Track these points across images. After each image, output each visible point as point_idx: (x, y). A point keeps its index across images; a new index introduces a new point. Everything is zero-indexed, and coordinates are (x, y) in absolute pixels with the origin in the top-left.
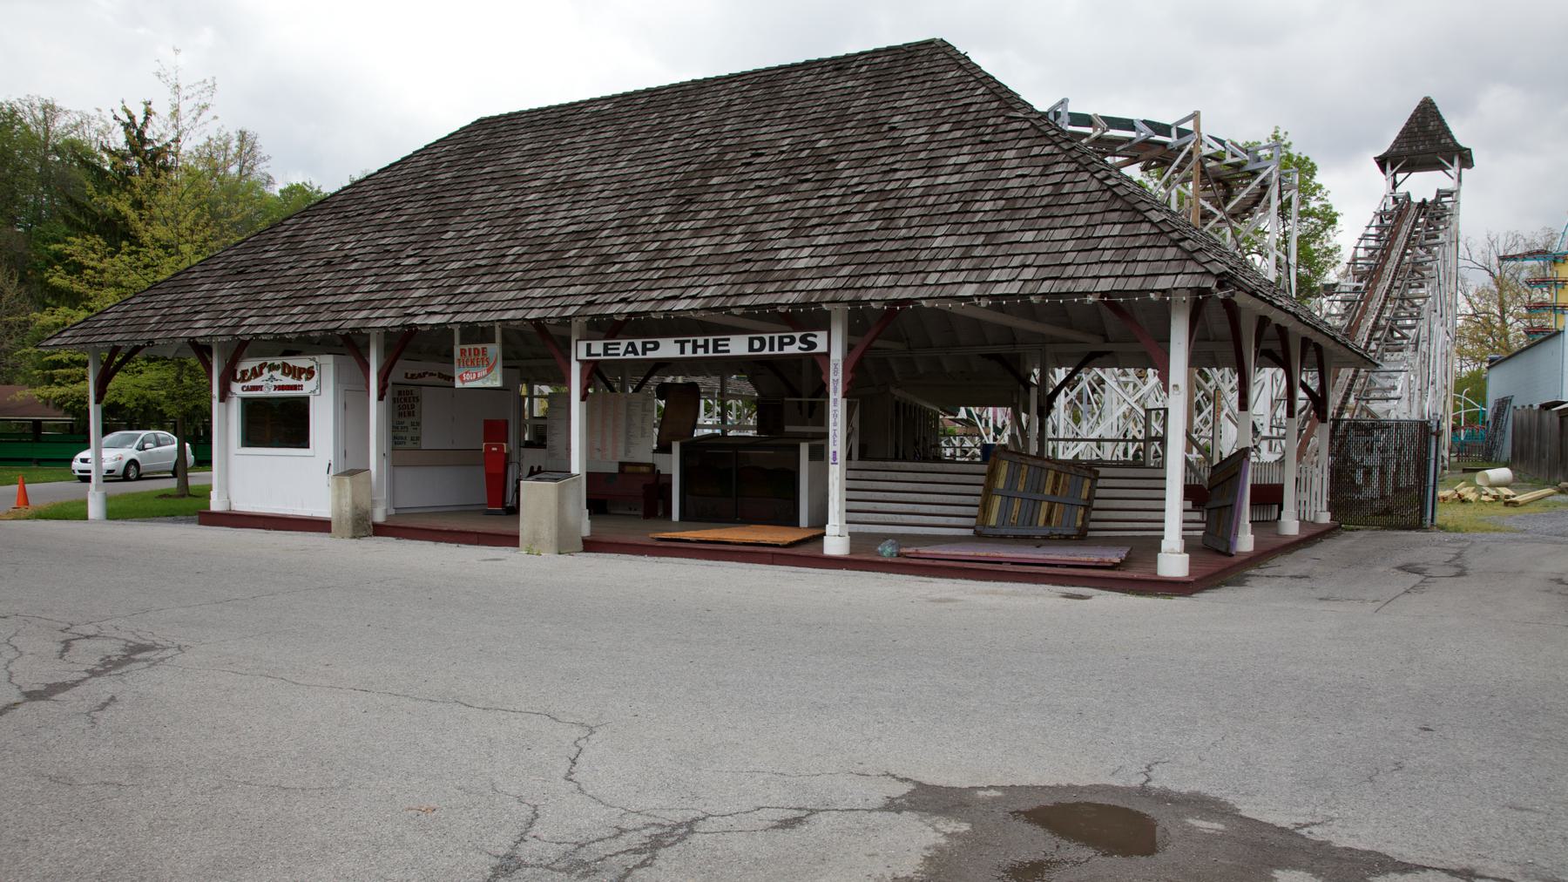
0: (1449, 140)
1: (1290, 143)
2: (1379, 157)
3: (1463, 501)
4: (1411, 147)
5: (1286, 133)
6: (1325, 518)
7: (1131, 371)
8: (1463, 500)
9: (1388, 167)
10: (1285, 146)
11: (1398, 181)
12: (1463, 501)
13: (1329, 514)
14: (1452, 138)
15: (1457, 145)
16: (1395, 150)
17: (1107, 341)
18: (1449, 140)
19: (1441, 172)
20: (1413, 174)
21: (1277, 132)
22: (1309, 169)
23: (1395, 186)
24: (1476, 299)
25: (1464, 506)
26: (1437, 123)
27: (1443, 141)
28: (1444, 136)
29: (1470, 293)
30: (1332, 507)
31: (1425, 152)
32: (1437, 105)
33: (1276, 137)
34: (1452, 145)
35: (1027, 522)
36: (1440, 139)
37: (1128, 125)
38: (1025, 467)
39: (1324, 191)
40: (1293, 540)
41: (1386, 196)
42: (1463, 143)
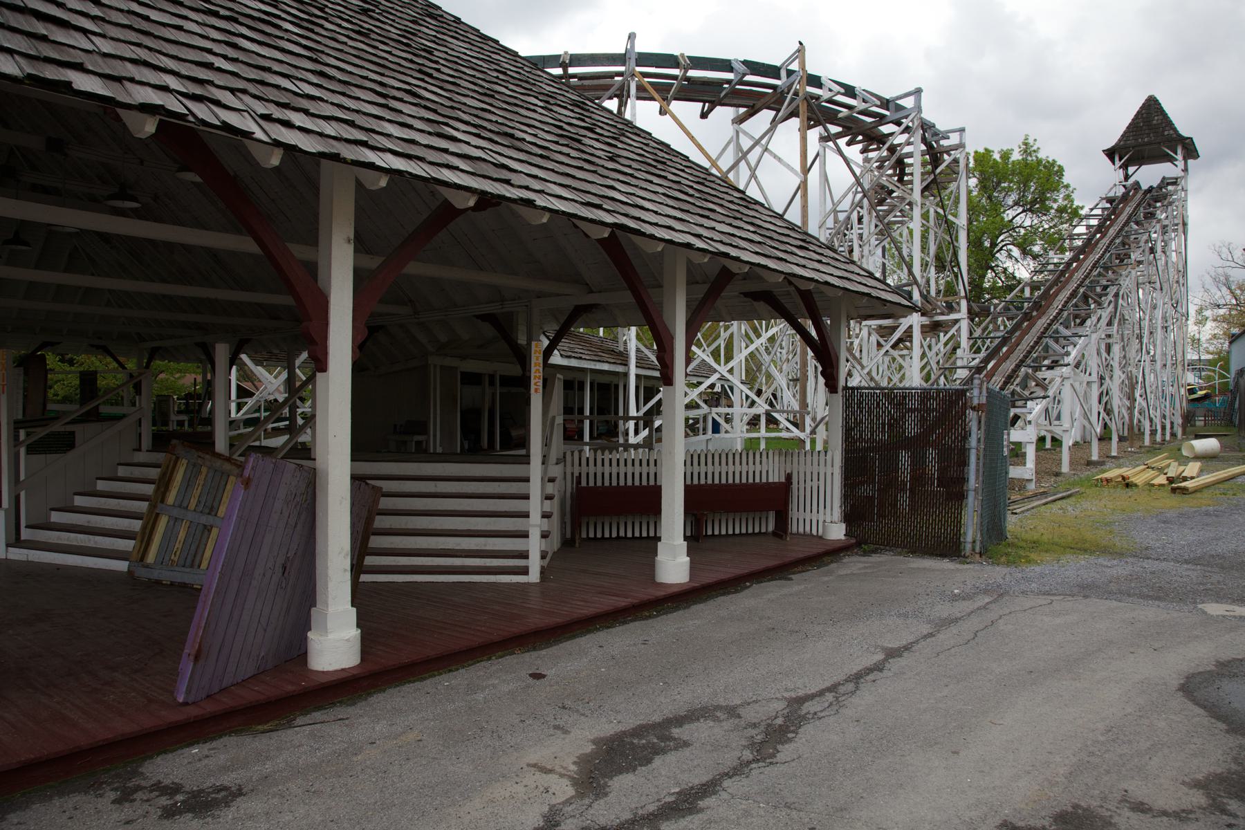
0: (1171, 132)
1: (1038, 148)
2: (1108, 150)
3: (1127, 485)
4: (1136, 140)
5: (1035, 140)
6: (837, 532)
7: (799, 336)
8: (1128, 484)
9: (1117, 158)
10: (1034, 151)
11: (1130, 173)
12: (1127, 485)
13: (843, 526)
14: (1175, 130)
15: (1180, 135)
16: (1122, 143)
17: (591, 292)
18: (1171, 132)
19: (1169, 164)
20: (1144, 167)
21: (1027, 139)
22: (1057, 172)
23: (1127, 177)
24: (1238, 292)
25: (1130, 492)
26: (1160, 117)
27: (1166, 133)
28: (1167, 128)
29: (1233, 288)
30: (850, 518)
31: (1150, 143)
32: (1160, 101)
33: (1026, 144)
34: (1175, 136)
35: (188, 563)
36: (1163, 131)
37: (725, 65)
38: (204, 470)
39: (1071, 189)
40: (324, 680)
41: (1115, 185)
42: (1184, 131)
